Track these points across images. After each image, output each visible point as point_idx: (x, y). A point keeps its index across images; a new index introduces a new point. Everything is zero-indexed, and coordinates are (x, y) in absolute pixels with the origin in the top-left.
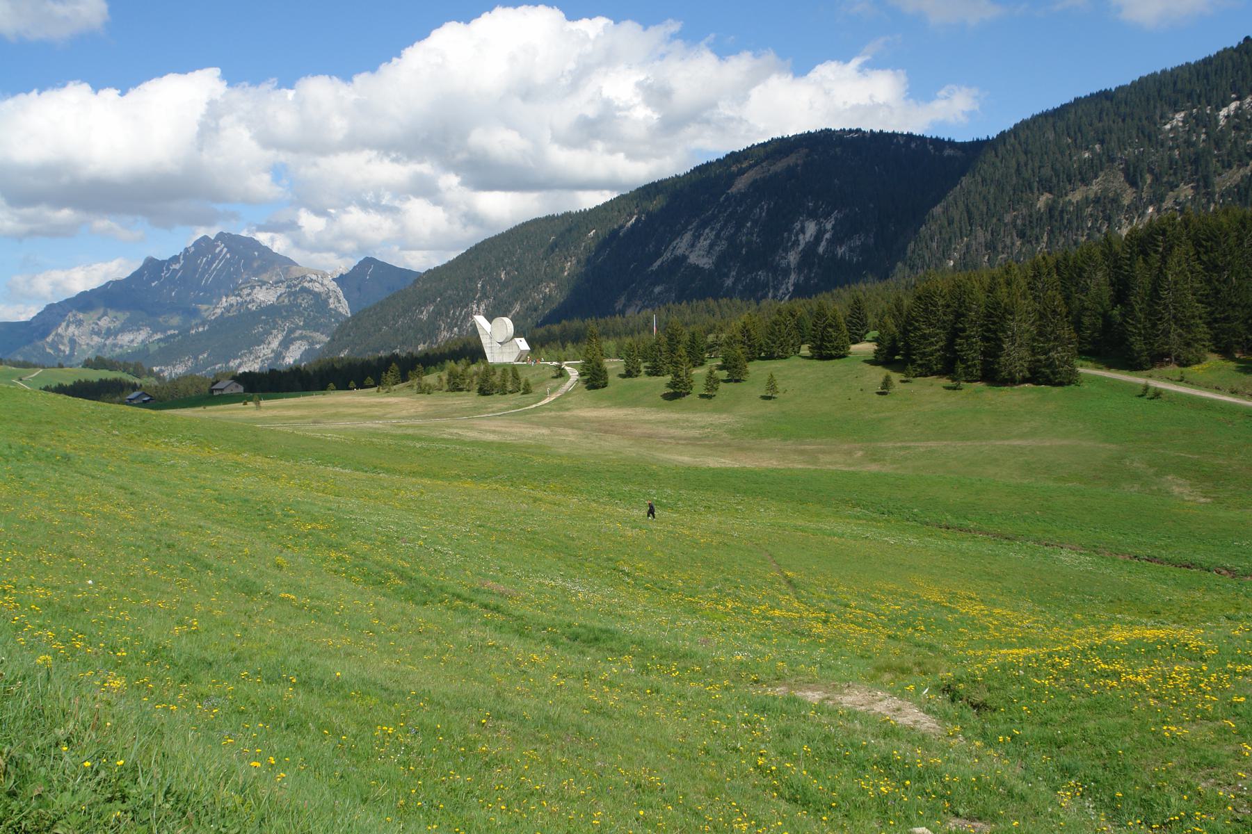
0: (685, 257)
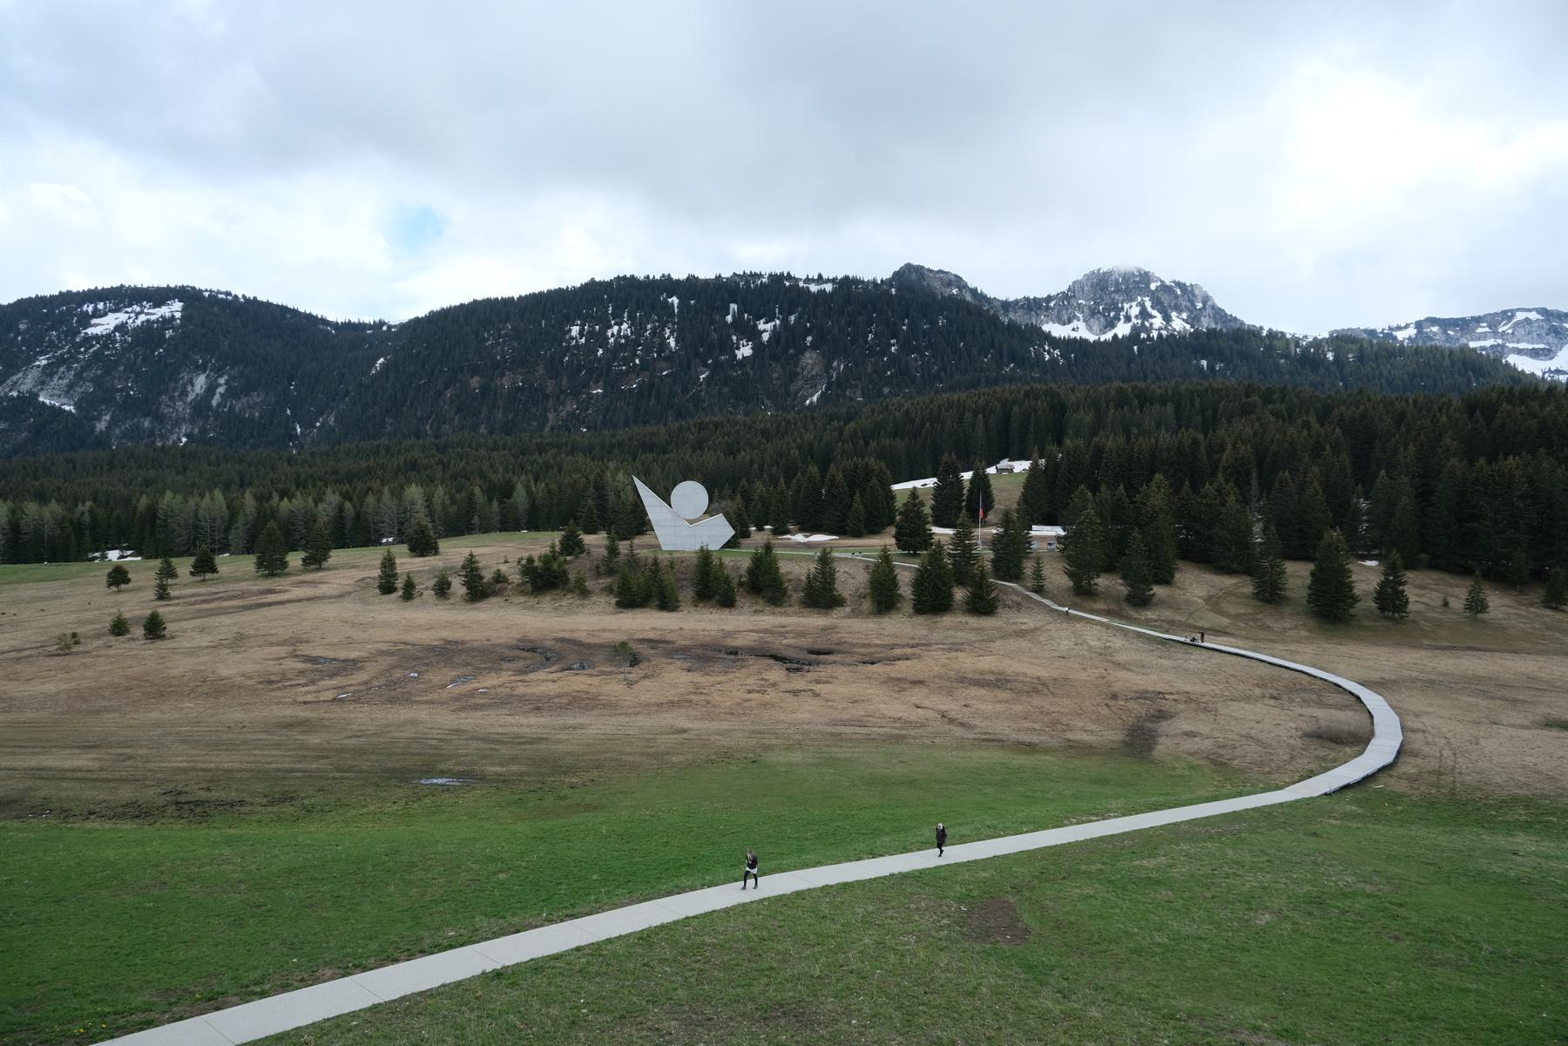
0: (35, 396)
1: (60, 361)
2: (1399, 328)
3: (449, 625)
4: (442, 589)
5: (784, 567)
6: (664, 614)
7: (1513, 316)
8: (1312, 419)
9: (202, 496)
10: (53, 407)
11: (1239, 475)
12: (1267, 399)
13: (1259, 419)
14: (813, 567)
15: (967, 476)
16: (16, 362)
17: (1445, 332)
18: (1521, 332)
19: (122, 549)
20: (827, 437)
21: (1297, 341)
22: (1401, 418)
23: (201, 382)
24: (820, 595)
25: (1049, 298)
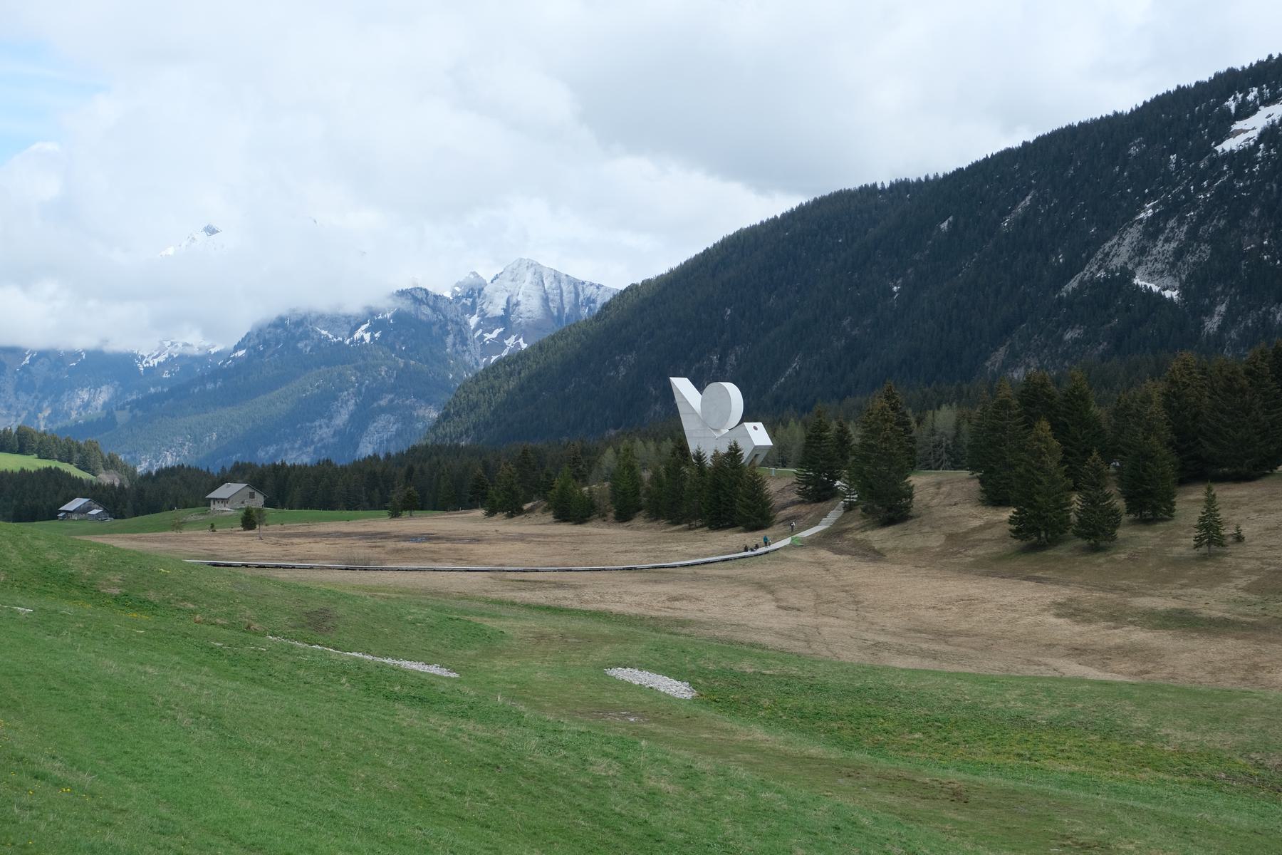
0: (1128, 275)
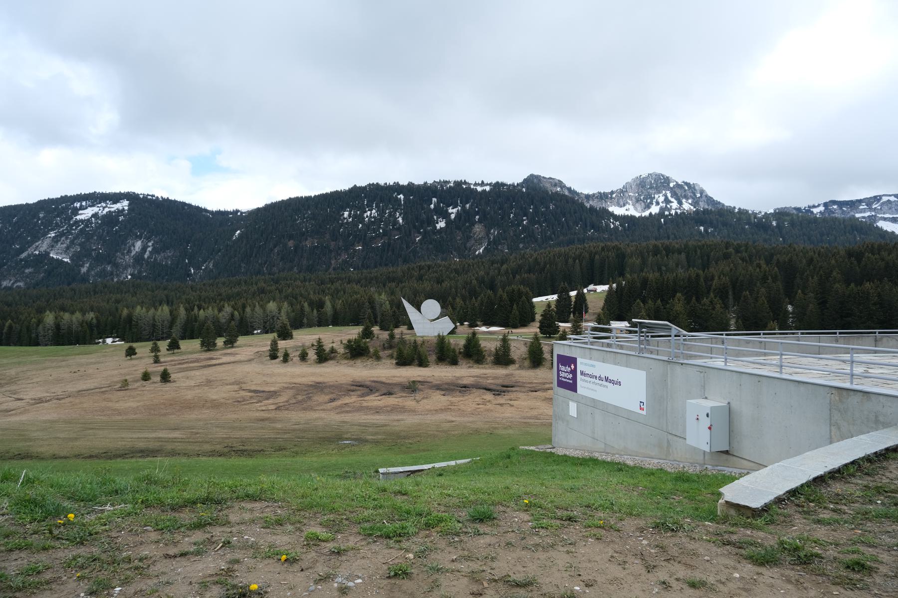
1: (62, 234)
2: (814, 207)
3: (313, 374)
4: (303, 357)
5: (483, 344)
6: (422, 369)
7: (881, 199)
8: (762, 262)
9: (156, 309)
10: (58, 260)
11: (722, 293)
12: (737, 250)
13: (733, 262)
14: (498, 344)
15: (573, 294)
16: (38, 235)
17: (841, 208)
18: (885, 208)
19: (114, 338)
20: (491, 273)
21: (755, 215)
22: (811, 261)
23: (138, 245)
24: (503, 358)
25: (612, 193)
